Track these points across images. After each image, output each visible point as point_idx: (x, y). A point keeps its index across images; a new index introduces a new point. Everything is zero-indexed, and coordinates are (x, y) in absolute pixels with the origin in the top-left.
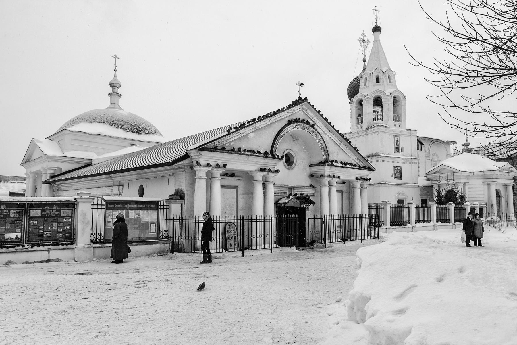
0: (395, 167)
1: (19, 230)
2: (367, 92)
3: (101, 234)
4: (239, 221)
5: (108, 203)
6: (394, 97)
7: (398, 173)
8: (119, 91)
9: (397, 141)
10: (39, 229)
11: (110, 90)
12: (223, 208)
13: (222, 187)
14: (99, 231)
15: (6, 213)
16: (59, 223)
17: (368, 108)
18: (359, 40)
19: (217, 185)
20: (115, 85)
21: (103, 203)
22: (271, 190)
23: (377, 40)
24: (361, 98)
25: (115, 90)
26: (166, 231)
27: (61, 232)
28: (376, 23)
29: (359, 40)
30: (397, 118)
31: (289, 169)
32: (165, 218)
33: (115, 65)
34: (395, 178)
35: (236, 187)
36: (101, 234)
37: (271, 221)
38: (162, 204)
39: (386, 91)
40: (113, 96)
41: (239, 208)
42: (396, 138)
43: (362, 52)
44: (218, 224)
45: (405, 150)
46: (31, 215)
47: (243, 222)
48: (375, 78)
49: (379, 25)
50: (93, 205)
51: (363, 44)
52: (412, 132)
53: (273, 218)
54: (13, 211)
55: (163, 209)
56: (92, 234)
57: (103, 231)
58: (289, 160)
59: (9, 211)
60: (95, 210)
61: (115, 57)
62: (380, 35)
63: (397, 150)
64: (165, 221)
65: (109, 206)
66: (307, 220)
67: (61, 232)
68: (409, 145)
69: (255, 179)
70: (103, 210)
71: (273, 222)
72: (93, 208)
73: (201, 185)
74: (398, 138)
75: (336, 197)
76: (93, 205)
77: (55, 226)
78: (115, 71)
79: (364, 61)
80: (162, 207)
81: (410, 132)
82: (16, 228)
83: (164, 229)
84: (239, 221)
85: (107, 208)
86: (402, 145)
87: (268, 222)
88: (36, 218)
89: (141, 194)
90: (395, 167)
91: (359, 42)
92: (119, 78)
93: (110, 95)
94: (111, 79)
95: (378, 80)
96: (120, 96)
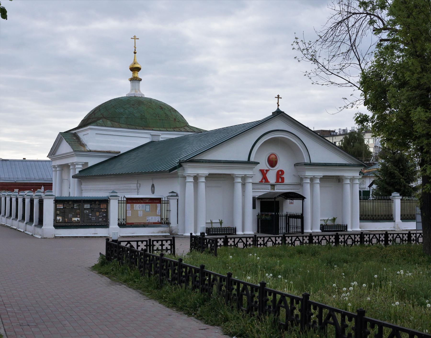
1: (79, 216)
3: (124, 219)
5: (128, 199)
10: (89, 216)
14: (122, 218)
15: (72, 206)
16: (99, 212)
19: (202, 186)
21: (125, 199)
25: (136, 75)
26: (167, 219)
27: (101, 218)
32: (166, 210)
36: (124, 219)
38: (164, 200)
46: (85, 207)
54: (75, 205)
56: (119, 219)
57: (125, 218)
59: (74, 204)
60: (120, 204)
61: (135, 38)
64: (166, 212)
65: (129, 201)
67: (101, 218)
70: (125, 204)
73: (190, 187)
77: (98, 214)
78: (135, 53)
80: (164, 202)
82: (77, 214)
83: (166, 217)
85: (127, 203)
88: (87, 209)
89: (153, 192)
92: (137, 60)
94: (129, 63)
96: (140, 80)
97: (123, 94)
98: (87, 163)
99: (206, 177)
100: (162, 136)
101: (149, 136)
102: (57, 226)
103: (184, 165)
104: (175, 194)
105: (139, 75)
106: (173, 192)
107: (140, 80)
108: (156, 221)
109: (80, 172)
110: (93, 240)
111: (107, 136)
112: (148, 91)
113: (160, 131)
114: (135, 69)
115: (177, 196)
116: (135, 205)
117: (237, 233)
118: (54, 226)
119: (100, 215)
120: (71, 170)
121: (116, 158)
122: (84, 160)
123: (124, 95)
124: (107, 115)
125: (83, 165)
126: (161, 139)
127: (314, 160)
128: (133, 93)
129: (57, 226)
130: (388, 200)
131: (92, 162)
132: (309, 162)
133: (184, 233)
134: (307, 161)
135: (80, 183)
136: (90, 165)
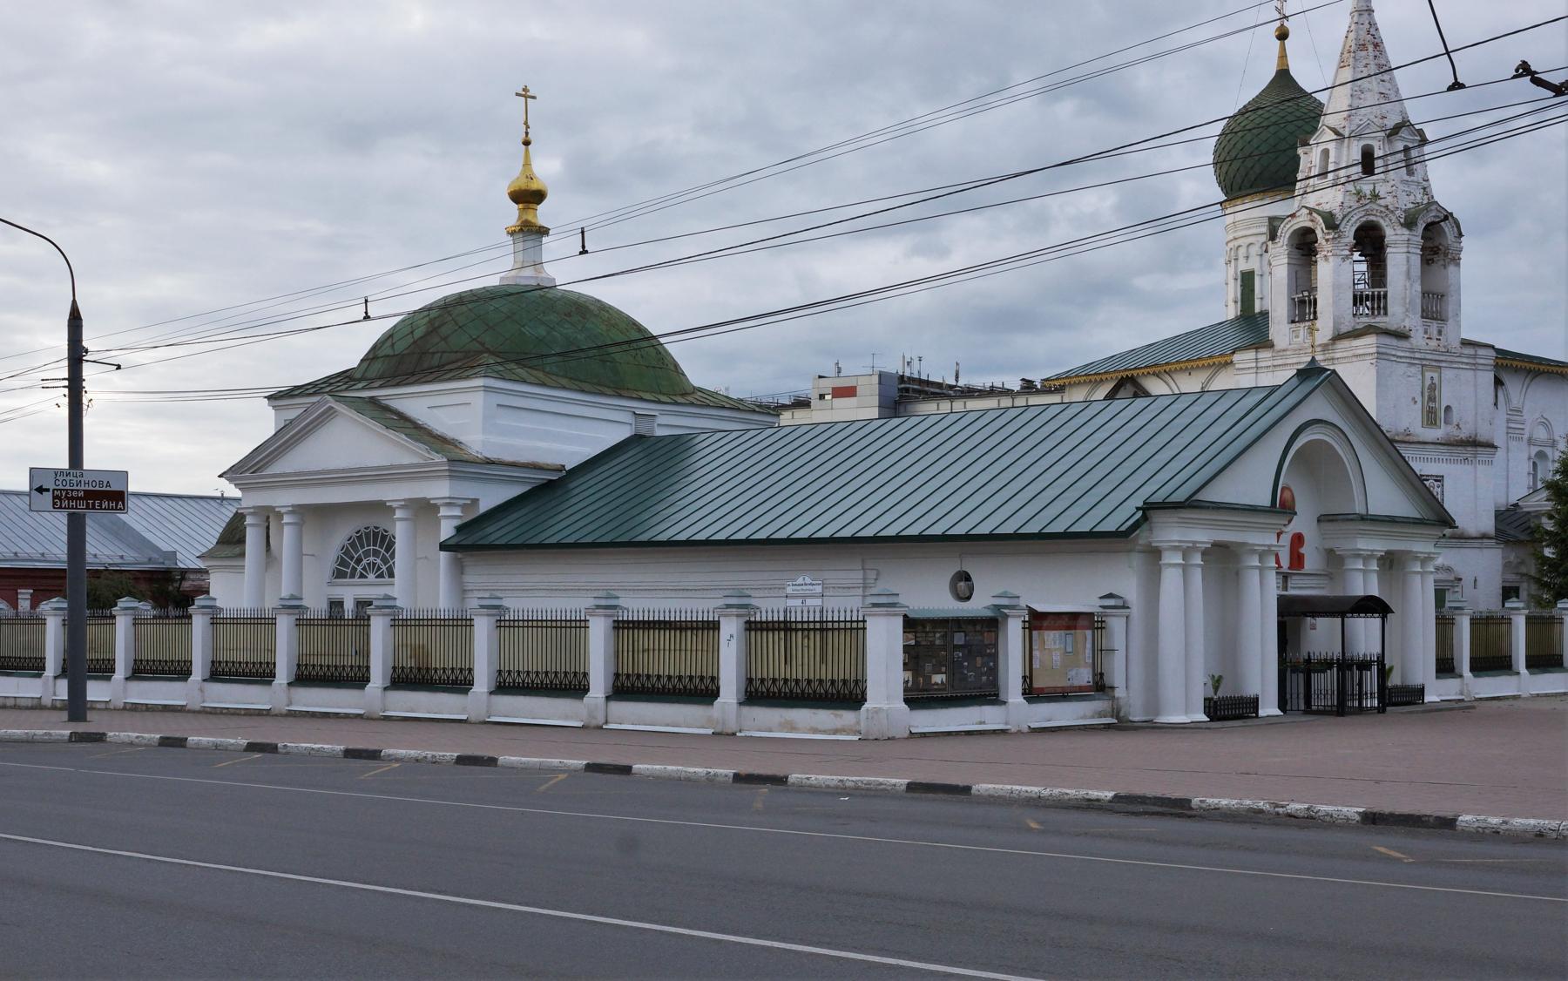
77: (979, 660)
96: (543, 231)
97: (490, 279)
98: (475, 501)
99: (1205, 553)
100: (662, 420)
101: (626, 417)
102: (917, 698)
103: (1157, 517)
104: (1120, 603)
105: (543, 214)
106: (1110, 596)
107: (543, 231)
108: (1084, 683)
109: (459, 529)
110: (951, 741)
111: (524, 414)
112: (564, 270)
113: (659, 402)
114: (528, 197)
115: (1124, 607)
116: (1047, 633)
117: (1262, 713)
118: (907, 701)
119: (983, 665)
120: (286, 529)
121: (549, 488)
122: (468, 490)
123: (493, 282)
124: (428, 347)
125: (464, 507)
126: (659, 432)
127: (1376, 509)
128: (528, 277)
129: (917, 698)
130: (106, 617)
131: (491, 496)
132: (1363, 512)
133: (1157, 714)
134: (1359, 509)
135: (458, 569)
136: (484, 507)
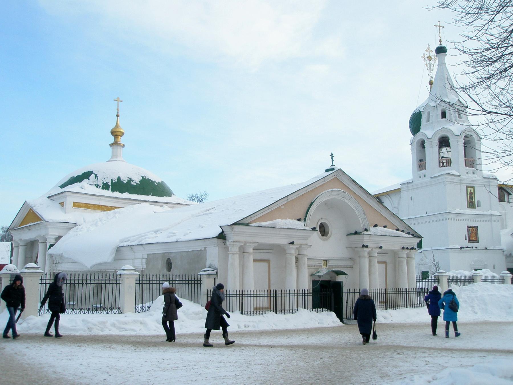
0: (469, 227)
2: (429, 132)
4: (272, 295)
6: (465, 137)
7: (473, 235)
8: (121, 140)
9: (471, 194)
11: (112, 139)
12: (380, 285)
13: (255, 261)
17: (432, 152)
18: (422, 57)
20: (117, 133)
22: (305, 262)
23: (442, 65)
24: (423, 138)
28: (440, 41)
29: (422, 57)
30: (470, 162)
31: (323, 240)
33: (118, 109)
34: (470, 241)
35: (268, 261)
37: (305, 296)
39: (455, 129)
40: (115, 147)
41: (271, 282)
42: (469, 189)
43: (428, 72)
44: (252, 298)
45: (482, 204)
47: (276, 297)
48: (440, 113)
49: (443, 44)
50: (41, 280)
51: (428, 62)
52: (490, 180)
53: (306, 292)
55: (188, 284)
58: (323, 230)
61: (118, 100)
62: (446, 57)
63: (471, 204)
66: (344, 295)
68: (487, 197)
69: (288, 252)
71: (306, 297)
72: (41, 283)
74: (472, 189)
75: (378, 269)
76: (41, 280)
79: (431, 83)
81: (487, 180)
84: (272, 295)
86: (477, 198)
87: (301, 297)
90: (469, 227)
91: (422, 59)
93: (111, 145)
95: (444, 115)
